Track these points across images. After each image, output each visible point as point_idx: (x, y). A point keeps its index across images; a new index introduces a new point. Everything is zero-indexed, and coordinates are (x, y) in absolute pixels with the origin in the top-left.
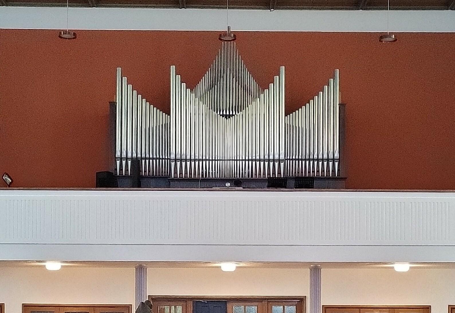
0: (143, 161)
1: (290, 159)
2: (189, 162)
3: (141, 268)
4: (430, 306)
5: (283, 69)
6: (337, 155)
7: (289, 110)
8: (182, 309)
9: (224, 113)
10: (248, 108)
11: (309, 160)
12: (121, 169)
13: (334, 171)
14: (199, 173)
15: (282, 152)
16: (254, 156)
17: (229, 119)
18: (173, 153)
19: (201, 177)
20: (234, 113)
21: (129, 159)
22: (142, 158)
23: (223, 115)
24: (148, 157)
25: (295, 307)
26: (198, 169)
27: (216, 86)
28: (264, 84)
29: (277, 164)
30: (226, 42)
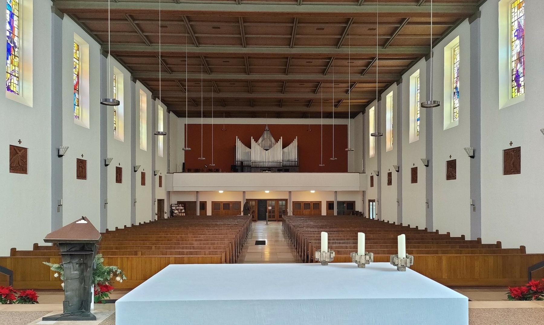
7: (284, 147)
28: (277, 141)
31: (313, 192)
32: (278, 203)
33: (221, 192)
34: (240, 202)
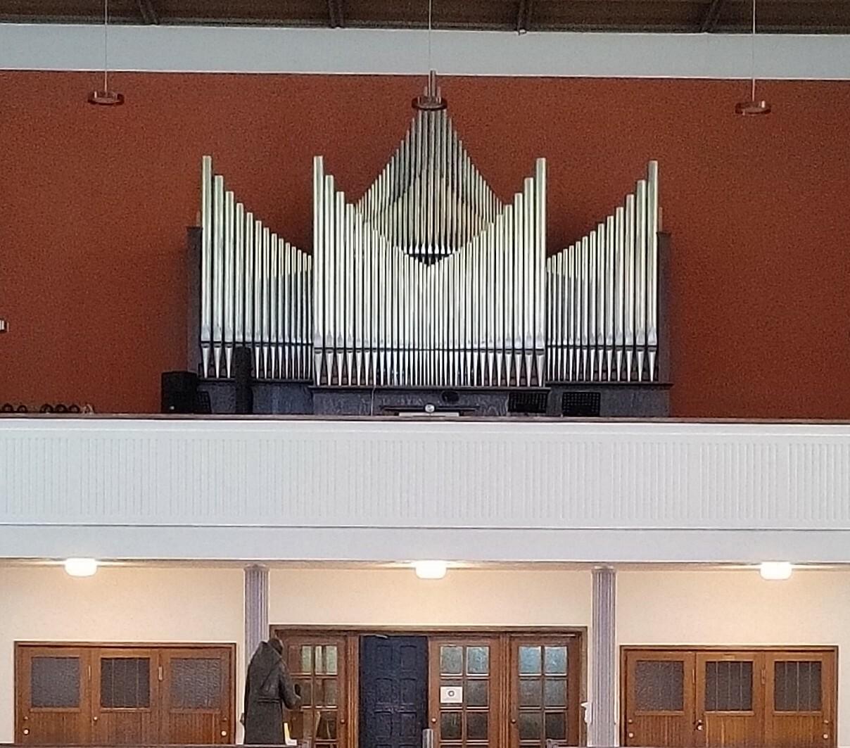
0: (257, 349)
1: (557, 347)
2: (352, 354)
3: (255, 573)
4: (837, 647)
5: (542, 163)
6: (653, 339)
7: (556, 244)
8: (339, 654)
9: (417, 251)
10: (471, 244)
12: (212, 365)
13: (646, 369)
14: (371, 376)
15: (541, 330)
16: (483, 342)
17: (433, 266)
18: (319, 336)
19: (375, 383)
20: (449, 252)
21: (229, 345)
22: (254, 343)
23: (414, 255)
24: (208, 338)
25: (566, 648)
26: (367, 368)
28: (505, 191)
29: (529, 358)
30: (433, 113)
31: (777, 570)
32: (512, 655)
33: (81, 567)
34: (230, 649)
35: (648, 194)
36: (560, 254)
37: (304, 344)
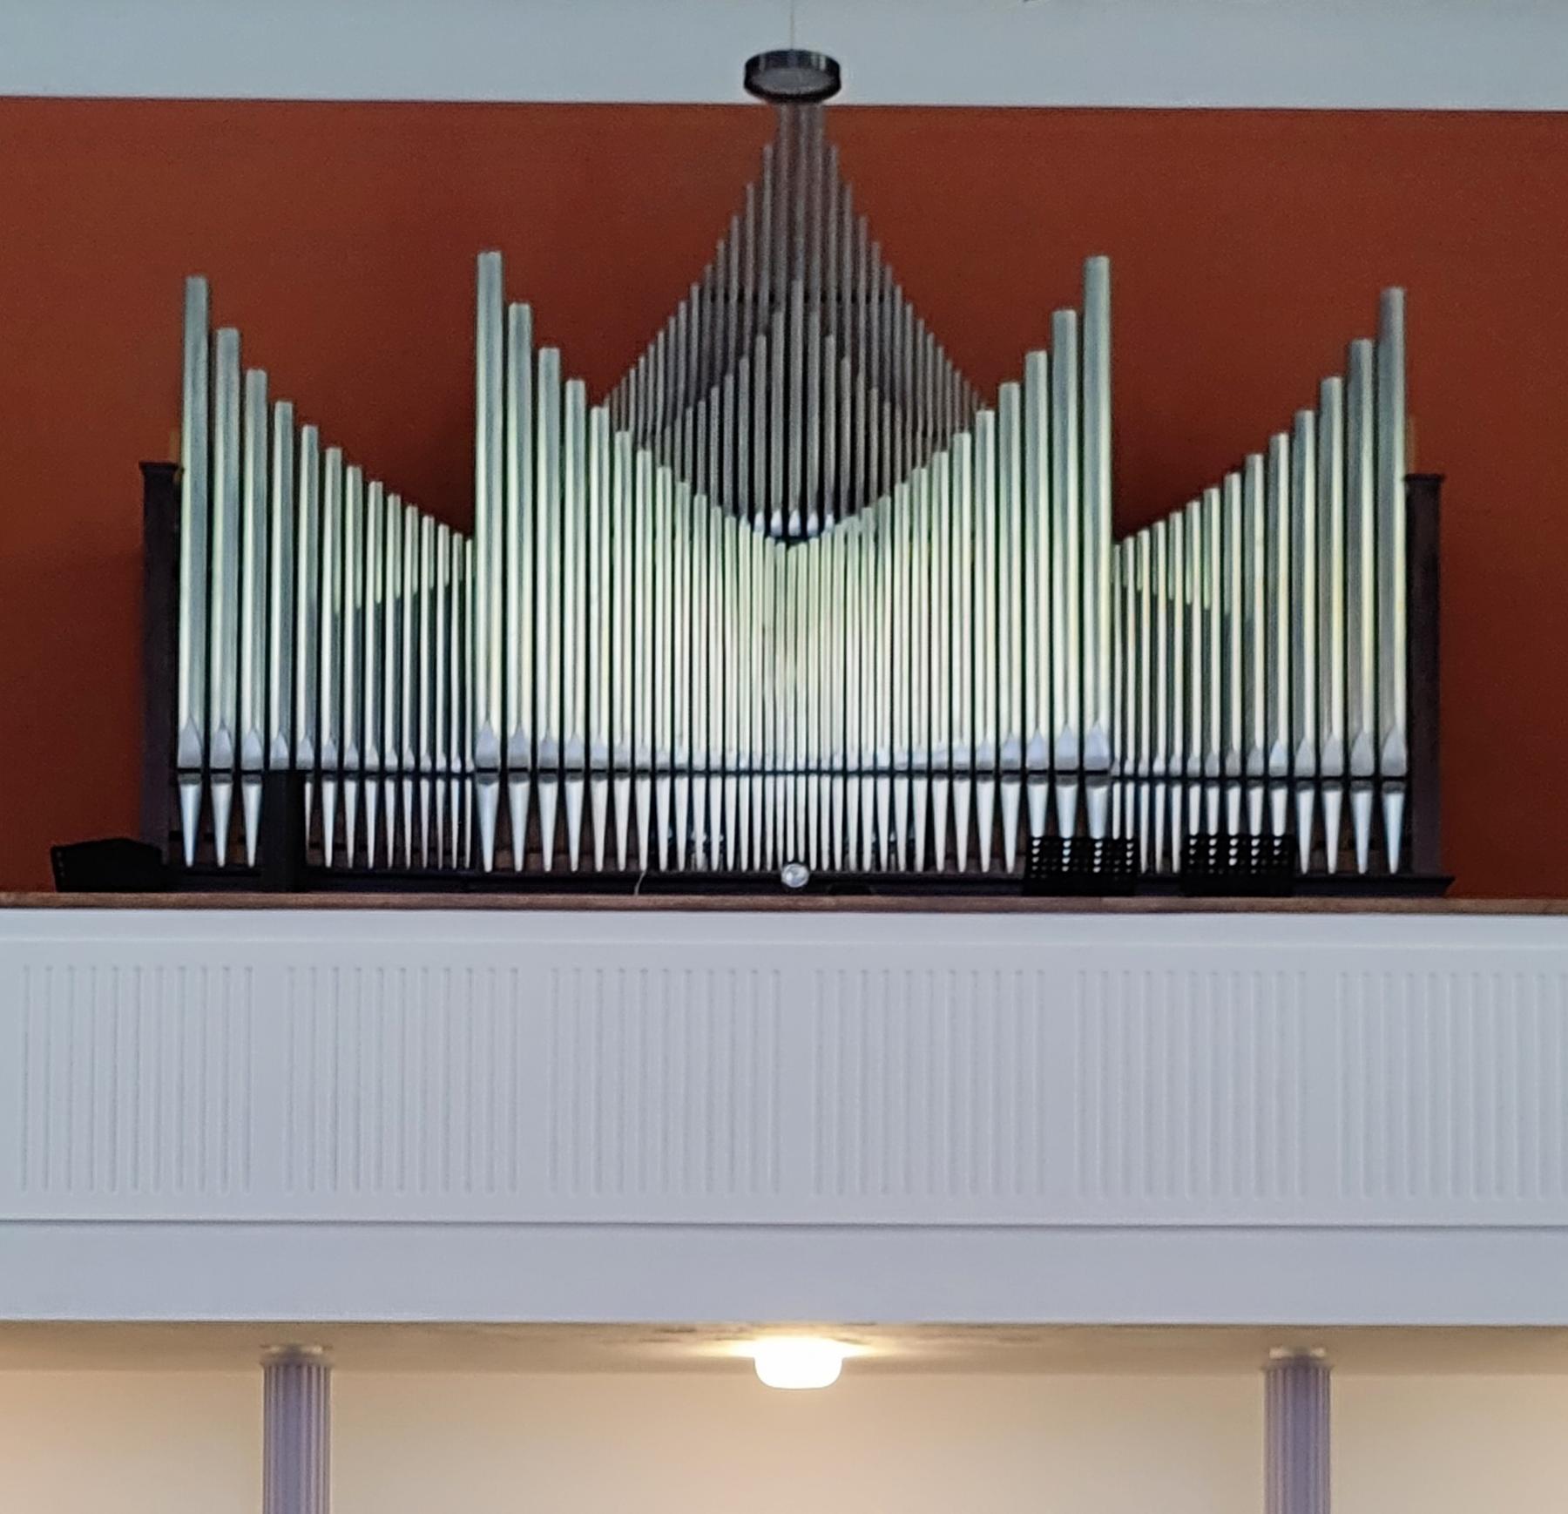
5: (1101, 267)
6: (1396, 752)
11: (1245, 781)
15: (1098, 728)
27: (729, 380)
35: (1385, 363)
36: (1145, 535)
37: (424, 775)
